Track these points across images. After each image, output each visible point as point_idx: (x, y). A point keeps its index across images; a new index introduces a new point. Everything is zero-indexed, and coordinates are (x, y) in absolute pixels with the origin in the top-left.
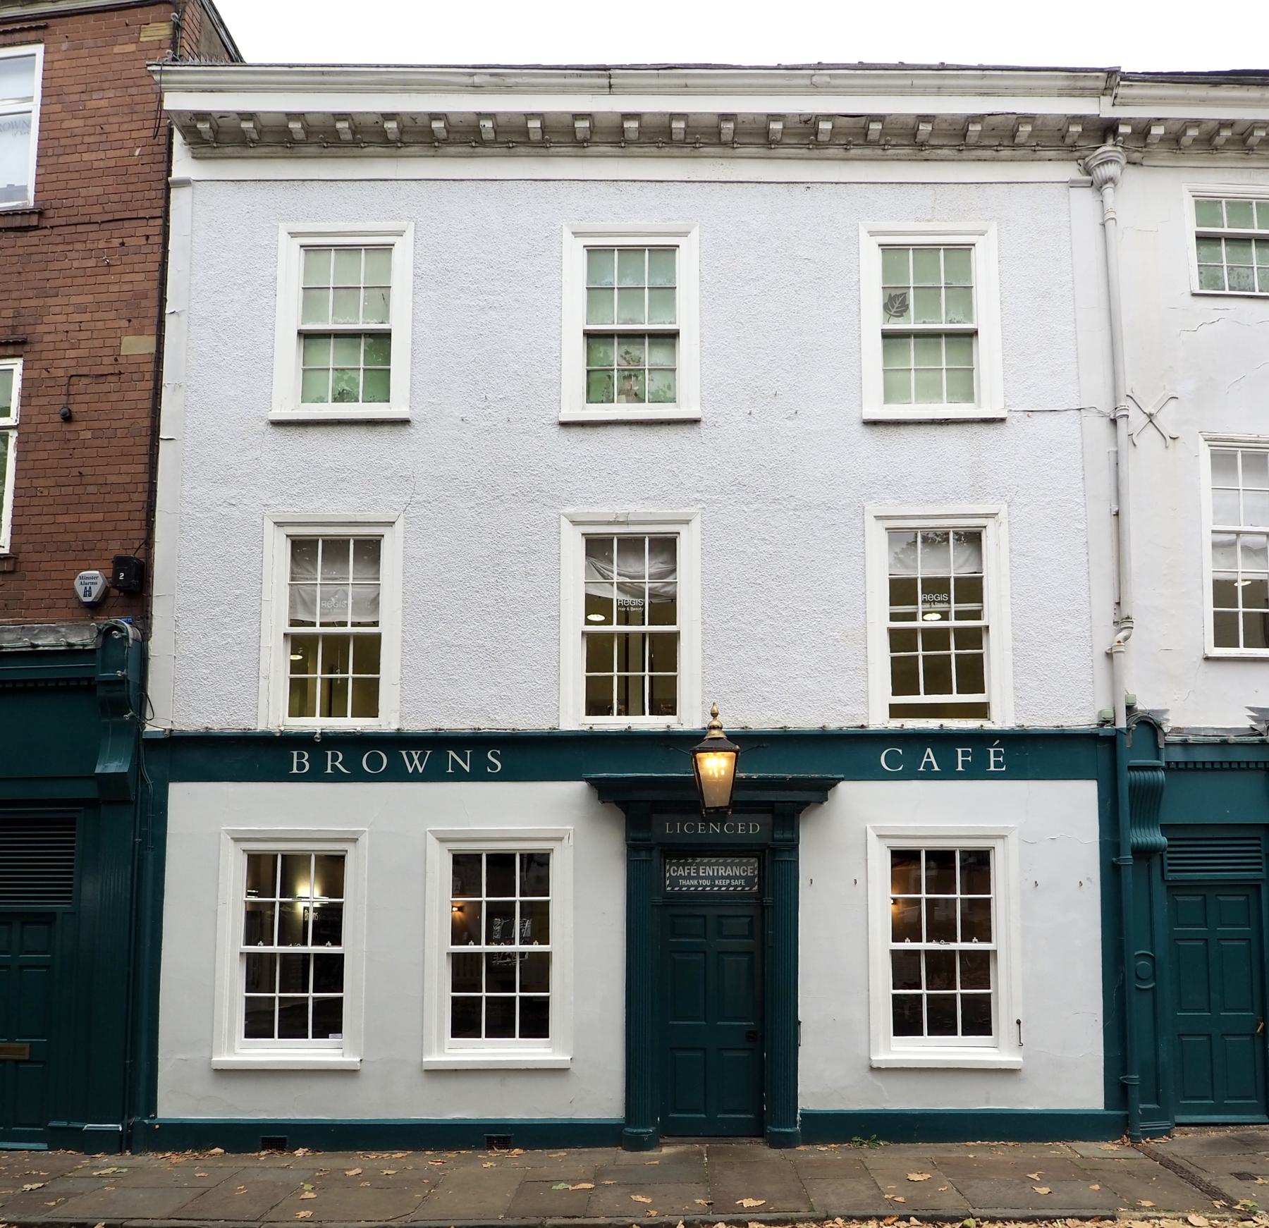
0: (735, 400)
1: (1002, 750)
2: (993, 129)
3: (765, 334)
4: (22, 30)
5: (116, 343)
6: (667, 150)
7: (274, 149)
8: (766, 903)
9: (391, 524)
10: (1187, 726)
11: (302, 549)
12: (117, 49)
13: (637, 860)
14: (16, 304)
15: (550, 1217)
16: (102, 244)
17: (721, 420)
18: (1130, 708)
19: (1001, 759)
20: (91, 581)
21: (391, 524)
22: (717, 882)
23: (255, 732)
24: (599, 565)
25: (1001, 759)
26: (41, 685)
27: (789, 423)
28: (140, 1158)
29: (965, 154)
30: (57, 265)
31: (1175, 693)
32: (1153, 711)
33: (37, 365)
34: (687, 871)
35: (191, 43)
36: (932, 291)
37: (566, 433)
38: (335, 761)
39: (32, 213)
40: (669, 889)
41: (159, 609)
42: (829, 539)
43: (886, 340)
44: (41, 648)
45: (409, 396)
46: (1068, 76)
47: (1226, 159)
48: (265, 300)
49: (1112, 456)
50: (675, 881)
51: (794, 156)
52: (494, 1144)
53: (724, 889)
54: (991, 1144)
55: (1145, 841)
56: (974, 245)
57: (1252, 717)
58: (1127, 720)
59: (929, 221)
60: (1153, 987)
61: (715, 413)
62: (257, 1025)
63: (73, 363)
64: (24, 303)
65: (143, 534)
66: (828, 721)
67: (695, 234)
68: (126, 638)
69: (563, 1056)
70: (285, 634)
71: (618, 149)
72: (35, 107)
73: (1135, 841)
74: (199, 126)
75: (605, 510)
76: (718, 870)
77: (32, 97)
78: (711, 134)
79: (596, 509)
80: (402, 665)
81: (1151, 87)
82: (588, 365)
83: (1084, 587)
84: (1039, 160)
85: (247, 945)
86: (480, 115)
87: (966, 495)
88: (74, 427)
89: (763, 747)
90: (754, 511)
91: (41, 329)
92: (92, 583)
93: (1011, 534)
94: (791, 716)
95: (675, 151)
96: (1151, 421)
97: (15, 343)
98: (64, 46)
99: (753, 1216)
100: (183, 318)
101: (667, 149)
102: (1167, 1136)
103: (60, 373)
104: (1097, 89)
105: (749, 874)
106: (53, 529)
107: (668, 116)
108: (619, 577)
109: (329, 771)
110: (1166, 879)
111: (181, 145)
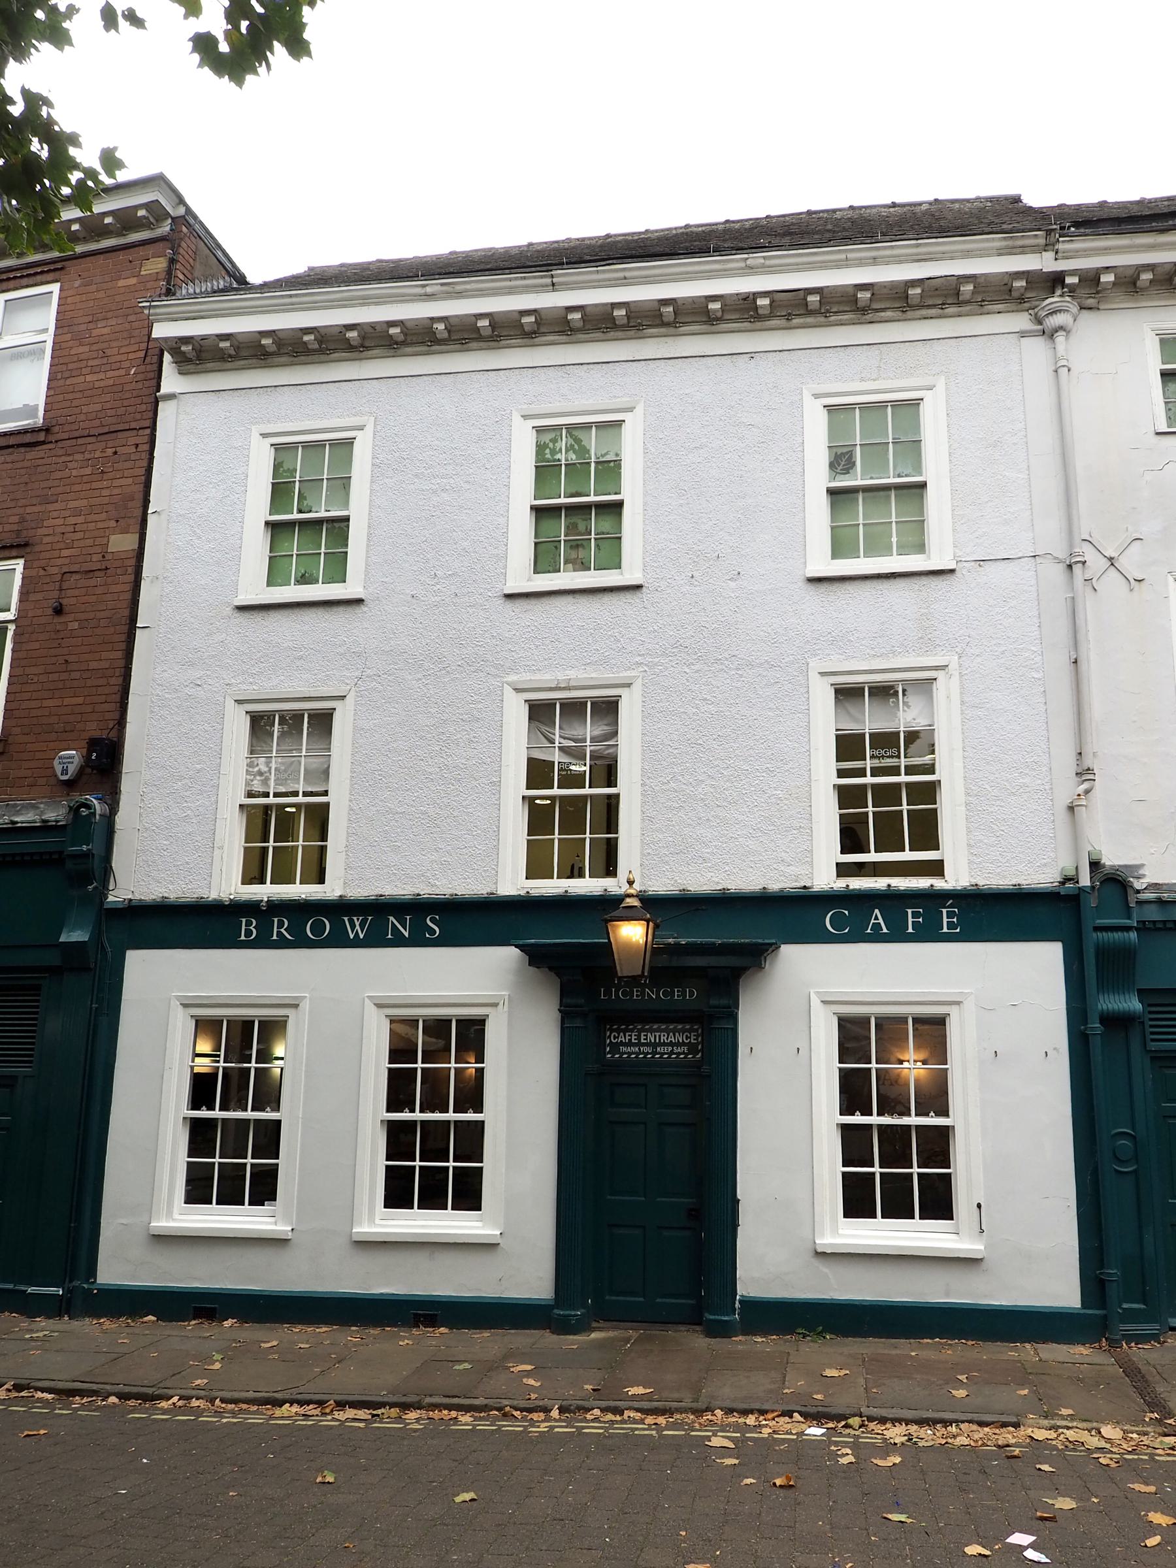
0: (678, 564)
1: (956, 910)
2: (937, 290)
3: (708, 499)
4: (42, 272)
5: (105, 541)
6: (612, 334)
7: (250, 361)
8: (703, 1072)
9: (343, 697)
10: (1166, 882)
11: (259, 724)
12: (121, 283)
13: (572, 1027)
14: (21, 511)
15: (431, 1396)
16: (98, 454)
17: (663, 584)
18: (1095, 865)
19: (955, 920)
20: (69, 760)
21: (343, 697)
22: (658, 1049)
23: (207, 901)
24: (544, 728)
25: (955, 920)
26: (8, 859)
27: (732, 584)
28: (76, 1323)
29: (910, 314)
30: (59, 475)
31: (1151, 847)
32: (1126, 866)
33: (36, 564)
34: (628, 1038)
35: (185, 272)
36: (880, 447)
37: (511, 605)
38: (280, 928)
39: (40, 430)
40: (609, 1056)
41: (126, 785)
42: (772, 697)
43: (833, 496)
44: (19, 825)
45: (363, 577)
46: (1005, 238)
48: (237, 496)
49: (1069, 601)
50: (615, 1047)
51: (736, 329)
52: (420, 1321)
53: (666, 1056)
54: (950, 1342)
55: (1116, 1007)
56: (922, 399)
58: (1091, 878)
59: (874, 380)
60: (1135, 1171)
61: (658, 578)
62: (198, 1192)
63: (67, 561)
64: (29, 510)
65: (117, 715)
66: (770, 882)
67: (639, 410)
68: (94, 814)
69: (493, 1230)
70: (240, 805)
71: (564, 337)
72: (49, 338)
73: (1105, 1007)
74: (183, 348)
75: (547, 677)
76: (660, 1036)
77: (48, 329)
78: (654, 316)
79: (538, 677)
80: (348, 833)
81: (1093, 240)
82: (535, 538)
83: (1042, 738)
84: (988, 314)
85: (192, 1109)
86: (432, 319)
87: (914, 648)
88: (62, 619)
89: (702, 910)
90: (695, 672)
91: (40, 531)
92: (69, 763)
93: (962, 687)
94: (732, 878)
95: (620, 334)
96: (1112, 564)
97: (19, 546)
98: (77, 284)
99: (631, 1403)
100: (164, 516)
101: (612, 333)
102: (1155, 1342)
103: (55, 570)
104: (1038, 246)
105: (692, 1041)
106: (39, 713)
107: (609, 306)
108: (562, 741)
109: (275, 937)
110: (1148, 1049)
111: (169, 364)
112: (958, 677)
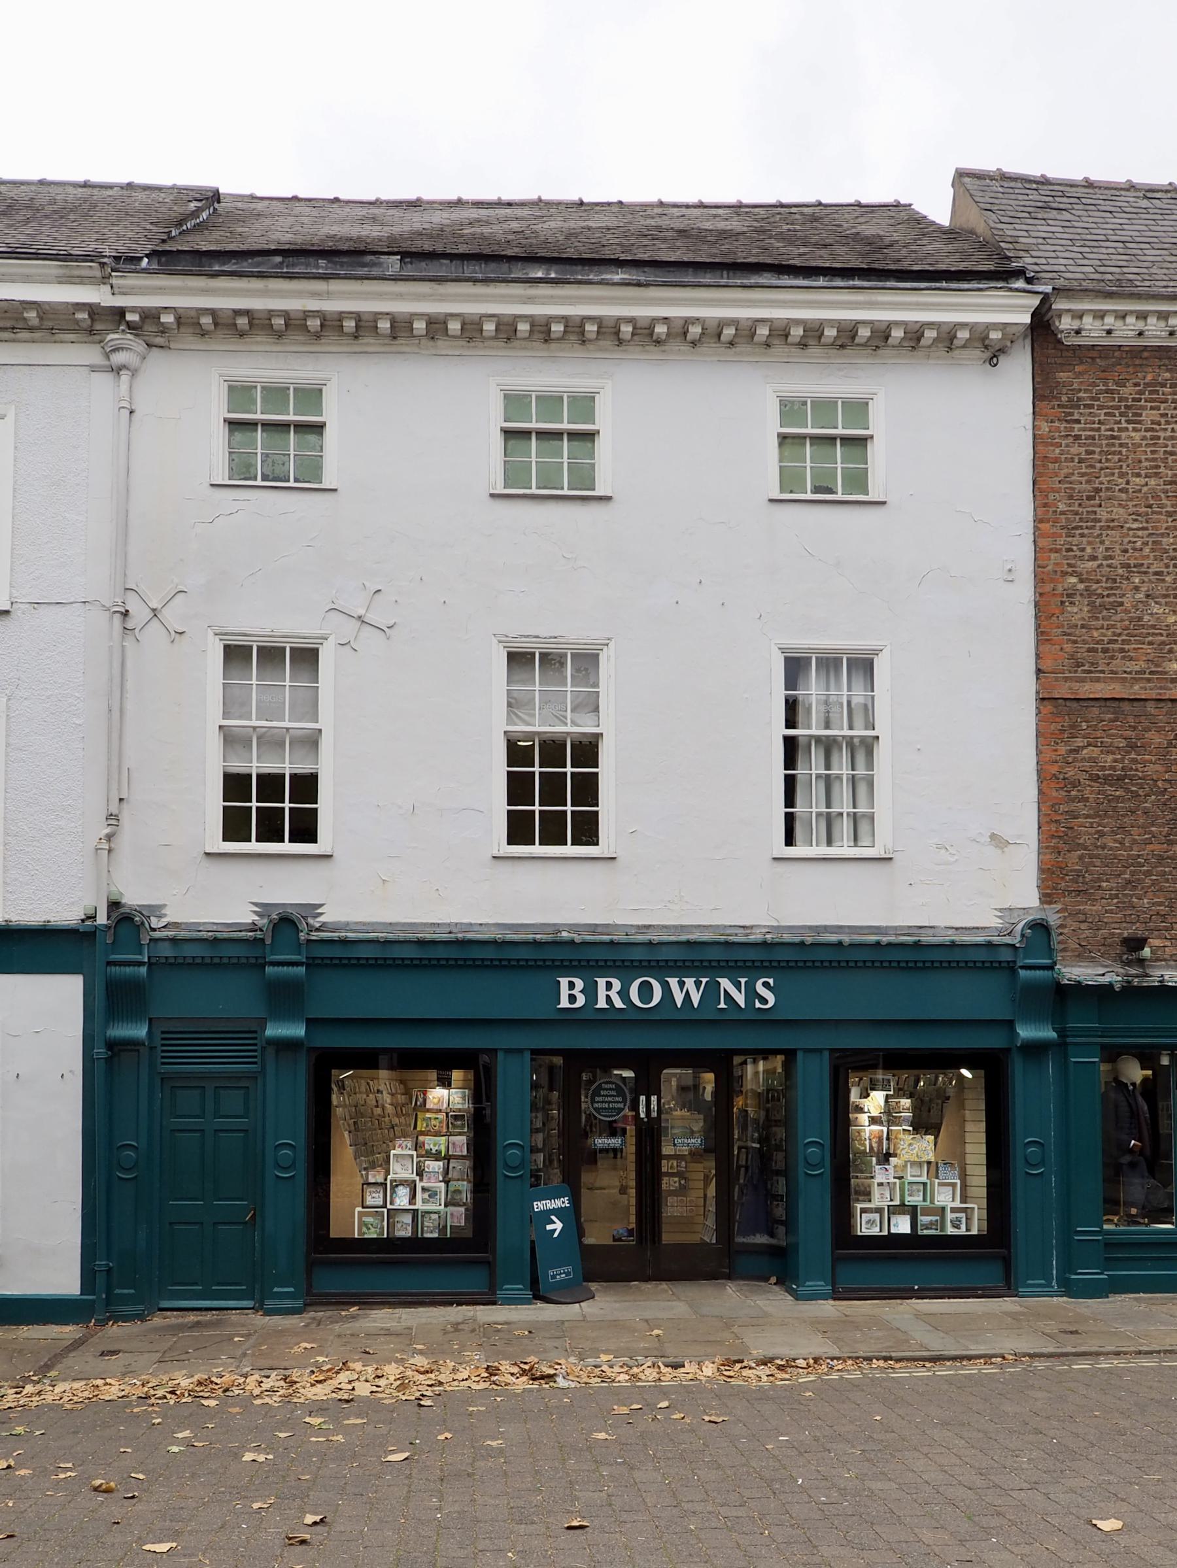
10: (185, 921)
11: (518, 660)
18: (114, 905)
32: (149, 906)
46: (61, 266)
47: (257, 343)
57: (255, 912)
60: (136, 1177)
112: (5, 718)
